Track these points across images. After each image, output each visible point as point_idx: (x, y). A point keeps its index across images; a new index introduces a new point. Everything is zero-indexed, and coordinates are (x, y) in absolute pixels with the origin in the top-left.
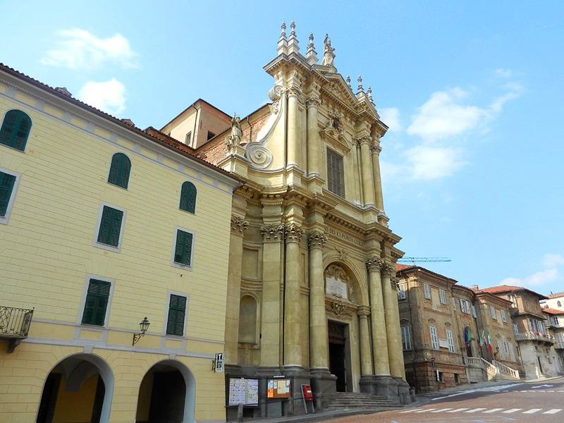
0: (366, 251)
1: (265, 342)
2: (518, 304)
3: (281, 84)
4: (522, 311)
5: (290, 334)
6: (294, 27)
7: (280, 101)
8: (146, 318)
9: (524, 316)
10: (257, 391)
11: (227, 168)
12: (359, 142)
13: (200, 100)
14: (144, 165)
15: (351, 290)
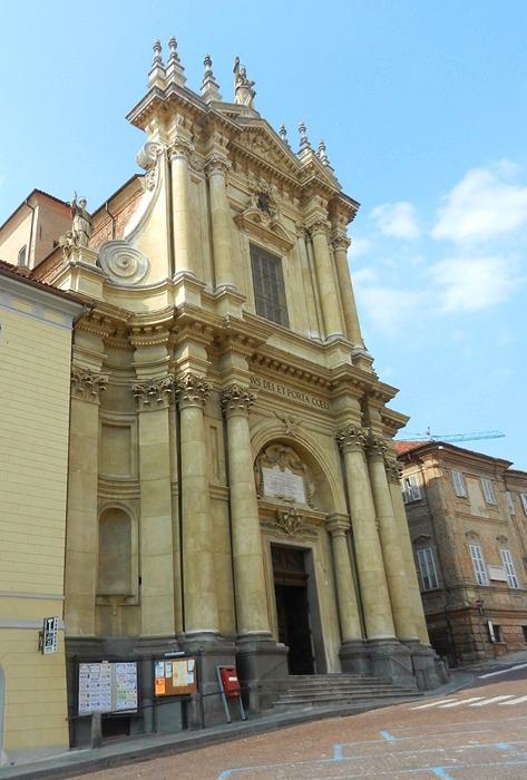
0: (334, 417)
1: (148, 590)
3: (156, 139)
6: (176, 47)
10: (135, 684)
12: (308, 234)
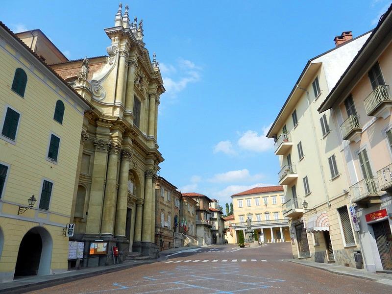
0: (146, 165)
1: (90, 217)
2: (200, 203)
3: (116, 45)
4: (201, 208)
5: (108, 213)
6: (128, 9)
7: (115, 57)
8: (33, 196)
9: (202, 211)
10: (83, 250)
11: (80, 93)
12: (149, 96)
13: (39, 31)
14: (35, 82)
15: (135, 188)
